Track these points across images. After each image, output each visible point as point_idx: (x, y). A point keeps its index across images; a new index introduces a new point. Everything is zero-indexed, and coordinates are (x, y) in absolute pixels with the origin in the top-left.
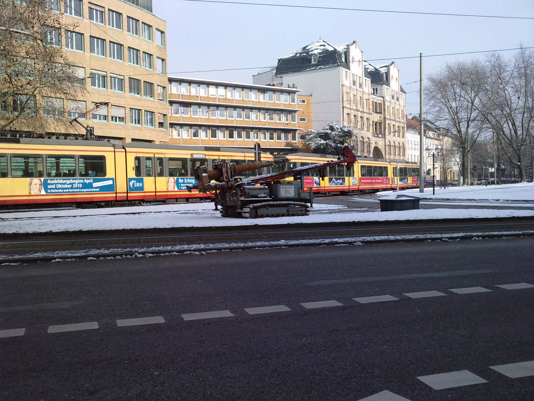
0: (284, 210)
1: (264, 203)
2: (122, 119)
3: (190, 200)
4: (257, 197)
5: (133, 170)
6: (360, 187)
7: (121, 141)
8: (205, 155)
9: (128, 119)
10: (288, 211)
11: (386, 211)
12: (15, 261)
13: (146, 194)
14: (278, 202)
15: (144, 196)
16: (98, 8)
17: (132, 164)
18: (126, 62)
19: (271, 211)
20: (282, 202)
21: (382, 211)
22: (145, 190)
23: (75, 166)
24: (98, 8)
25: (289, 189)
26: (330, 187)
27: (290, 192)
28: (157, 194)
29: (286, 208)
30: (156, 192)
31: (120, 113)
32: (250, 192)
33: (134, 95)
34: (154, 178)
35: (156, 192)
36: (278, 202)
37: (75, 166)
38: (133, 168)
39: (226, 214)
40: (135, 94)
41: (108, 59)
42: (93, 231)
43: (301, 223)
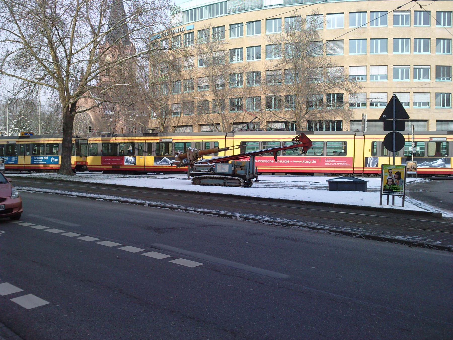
0: (221, 182)
1: (203, 176)
2: (426, 104)
3: (275, 174)
4: (200, 171)
5: (370, 151)
6: (364, 169)
7: (426, 123)
8: (447, 138)
9: (433, 104)
10: (225, 183)
11: (359, 191)
12: (198, 212)
13: (19, 166)
14: (215, 176)
15: (18, 167)
16: (403, 13)
17: (368, 146)
18: (433, 53)
19: (211, 181)
20: (217, 176)
21: (330, 190)
22: (19, 163)
23: (425, 145)
24: (403, 13)
25: (224, 167)
26: (156, 166)
27: (225, 169)
28: (25, 166)
29: (222, 180)
30: (24, 165)
31: (425, 98)
32: (196, 168)
33: (444, 81)
34: (389, 157)
35: (24, 165)
36: (215, 176)
37: (425, 145)
38: (370, 150)
39: (195, 182)
40: (444, 79)
41: (412, 54)
42: (163, 189)
43: (156, 188)
